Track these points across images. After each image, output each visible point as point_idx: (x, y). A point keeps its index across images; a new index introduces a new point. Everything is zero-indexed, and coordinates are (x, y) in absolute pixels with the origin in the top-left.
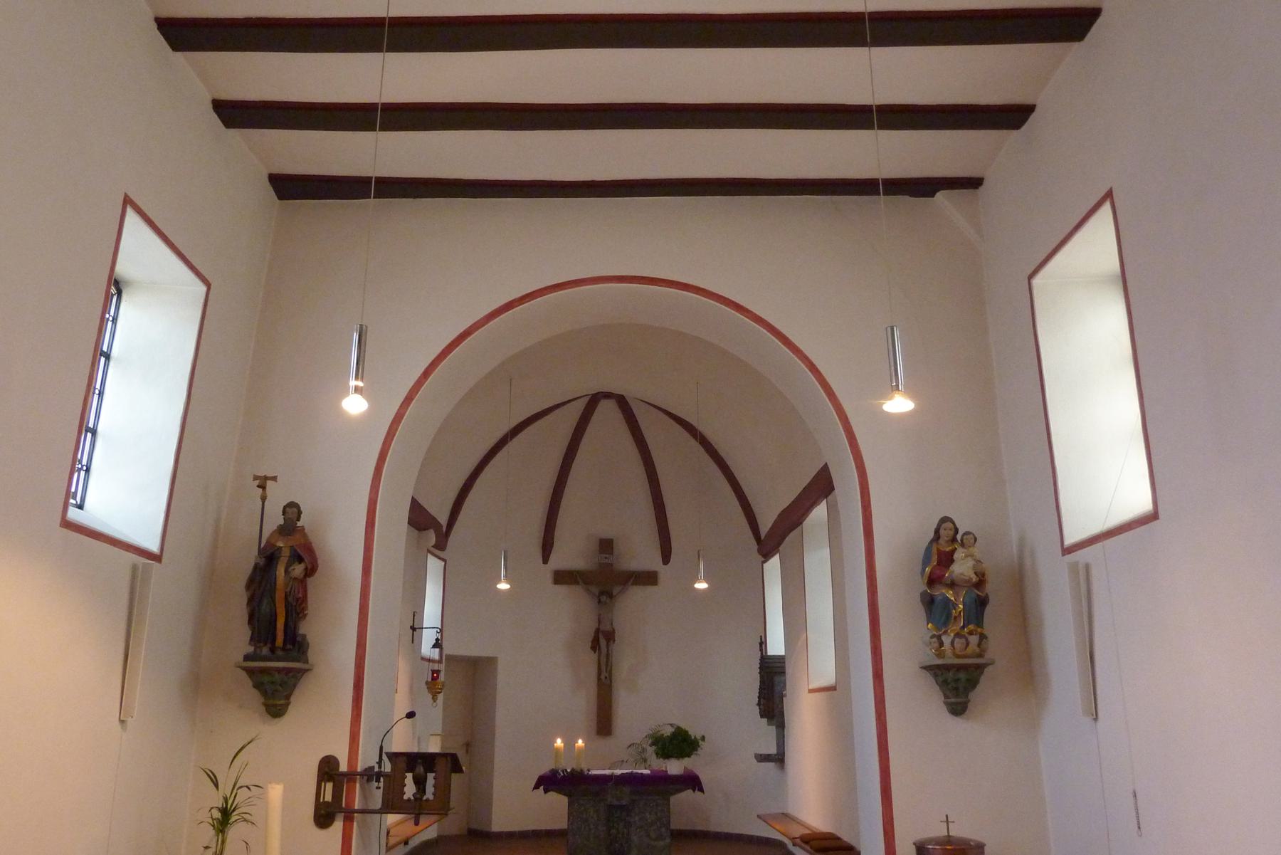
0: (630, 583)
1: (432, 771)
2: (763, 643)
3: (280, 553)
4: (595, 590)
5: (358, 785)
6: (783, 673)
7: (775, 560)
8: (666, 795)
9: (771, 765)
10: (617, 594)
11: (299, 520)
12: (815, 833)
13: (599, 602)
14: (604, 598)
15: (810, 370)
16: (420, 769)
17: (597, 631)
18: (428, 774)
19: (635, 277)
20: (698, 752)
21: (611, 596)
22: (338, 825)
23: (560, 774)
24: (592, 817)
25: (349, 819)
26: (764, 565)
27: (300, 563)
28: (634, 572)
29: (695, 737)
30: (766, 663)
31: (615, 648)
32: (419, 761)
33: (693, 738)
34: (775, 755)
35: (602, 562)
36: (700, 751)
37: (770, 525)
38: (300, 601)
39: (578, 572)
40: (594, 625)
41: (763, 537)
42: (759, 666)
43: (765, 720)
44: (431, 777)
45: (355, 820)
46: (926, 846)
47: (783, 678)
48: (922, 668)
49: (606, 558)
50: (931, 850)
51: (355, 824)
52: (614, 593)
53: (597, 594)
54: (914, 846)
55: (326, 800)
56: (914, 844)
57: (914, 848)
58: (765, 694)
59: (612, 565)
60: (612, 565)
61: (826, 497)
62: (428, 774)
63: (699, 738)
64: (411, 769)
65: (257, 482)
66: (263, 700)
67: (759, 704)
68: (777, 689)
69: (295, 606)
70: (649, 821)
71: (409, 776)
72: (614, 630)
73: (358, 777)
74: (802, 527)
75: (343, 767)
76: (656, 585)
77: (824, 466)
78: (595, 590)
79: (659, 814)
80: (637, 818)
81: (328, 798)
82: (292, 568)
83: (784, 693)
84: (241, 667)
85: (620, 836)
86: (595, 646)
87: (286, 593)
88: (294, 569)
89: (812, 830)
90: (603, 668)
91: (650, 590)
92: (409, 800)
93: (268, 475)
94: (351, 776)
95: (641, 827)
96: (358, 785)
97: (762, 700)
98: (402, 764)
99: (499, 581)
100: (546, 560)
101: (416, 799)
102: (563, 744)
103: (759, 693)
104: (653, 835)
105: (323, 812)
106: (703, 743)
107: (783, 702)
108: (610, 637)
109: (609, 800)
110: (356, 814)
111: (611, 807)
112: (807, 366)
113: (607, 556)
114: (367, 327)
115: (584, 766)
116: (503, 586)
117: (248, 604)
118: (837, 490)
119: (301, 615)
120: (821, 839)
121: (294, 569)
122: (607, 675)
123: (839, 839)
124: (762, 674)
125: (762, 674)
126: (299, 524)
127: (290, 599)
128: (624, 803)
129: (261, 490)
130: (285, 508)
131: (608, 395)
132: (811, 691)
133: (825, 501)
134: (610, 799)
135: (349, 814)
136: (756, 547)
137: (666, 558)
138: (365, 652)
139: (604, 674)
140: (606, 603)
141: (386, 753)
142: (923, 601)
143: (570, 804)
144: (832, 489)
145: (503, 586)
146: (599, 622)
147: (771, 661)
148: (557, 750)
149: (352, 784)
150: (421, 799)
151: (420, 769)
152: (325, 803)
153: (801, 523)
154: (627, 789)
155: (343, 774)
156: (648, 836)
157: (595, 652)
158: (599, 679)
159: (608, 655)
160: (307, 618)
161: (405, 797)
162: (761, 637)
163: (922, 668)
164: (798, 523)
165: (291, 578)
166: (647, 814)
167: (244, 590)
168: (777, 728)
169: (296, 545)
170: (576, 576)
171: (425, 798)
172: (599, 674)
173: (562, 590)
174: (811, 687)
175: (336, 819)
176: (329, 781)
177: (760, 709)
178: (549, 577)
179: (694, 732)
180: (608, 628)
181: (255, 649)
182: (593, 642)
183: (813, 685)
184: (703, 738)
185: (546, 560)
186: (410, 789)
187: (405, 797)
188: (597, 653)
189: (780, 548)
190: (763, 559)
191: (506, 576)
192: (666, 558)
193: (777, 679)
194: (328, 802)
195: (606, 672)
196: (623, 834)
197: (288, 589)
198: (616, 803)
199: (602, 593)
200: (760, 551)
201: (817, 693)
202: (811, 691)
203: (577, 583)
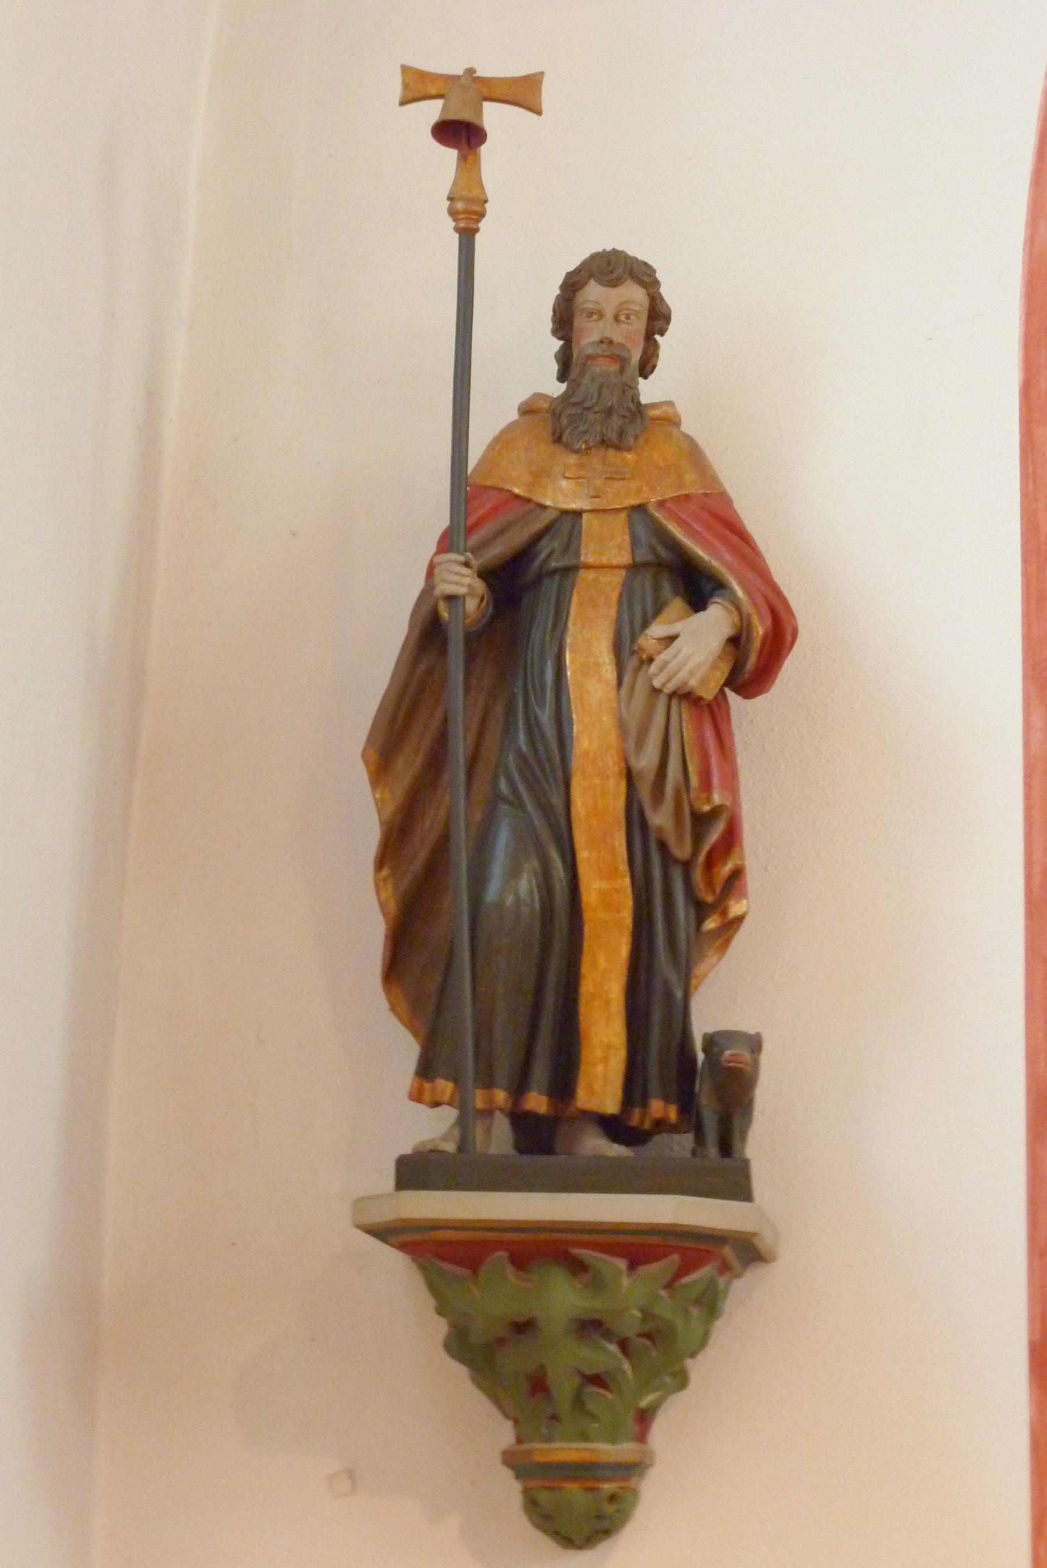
3: (572, 543)
11: (646, 368)
27: (697, 603)
38: (714, 835)
65: (432, 111)
66: (505, 1434)
69: (687, 866)
76: (752, 1202)
82: (658, 629)
84: (382, 1233)
87: (630, 776)
88: (672, 639)
93: (486, 70)
117: (380, 863)
119: (711, 924)
121: (672, 639)
126: (649, 391)
127: (660, 819)
129: (451, 154)
130: (572, 285)
142: (520, 1444)
160: (741, 938)
165: (656, 692)
167: (360, 775)
169: (661, 504)
181: (462, 1123)
197: (646, 761)
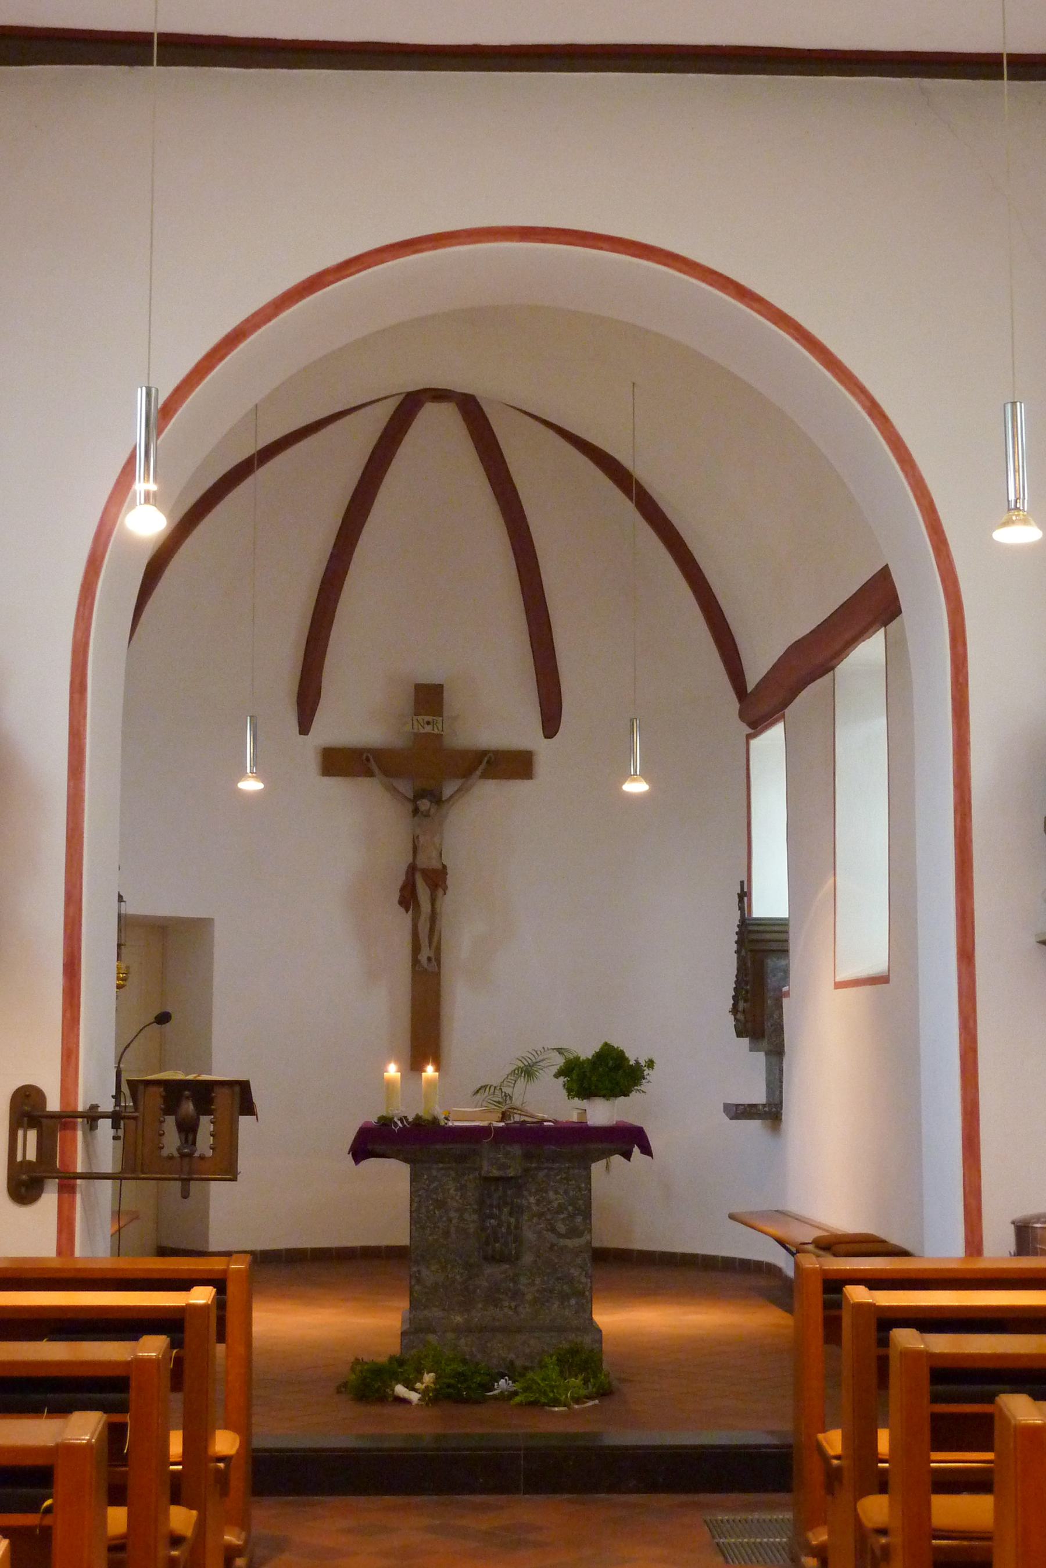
0: (478, 773)
1: (209, 1112)
2: (744, 896)
4: (405, 787)
5: (80, 1134)
6: (784, 952)
7: (774, 736)
8: (585, 1161)
9: (754, 1126)
10: (451, 797)
12: (836, 1236)
13: (416, 811)
14: (424, 804)
15: (870, 415)
16: (188, 1107)
17: (412, 869)
18: (201, 1117)
19: (548, 229)
20: (642, 1088)
21: (438, 800)
22: (49, 1199)
23: (396, 1124)
24: (452, 1198)
25: (67, 1184)
26: (754, 743)
28: (485, 753)
29: (637, 1062)
30: (750, 932)
31: (448, 903)
32: (187, 1093)
33: (632, 1062)
34: (764, 1105)
35: (422, 731)
36: (645, 1086)
37: (764, 671)
39: (369, 750)
40: (410, 860)
41: (750, 687)
42: (736, 938)
43: (745, 1041)
44: (205, 1121)
45: (78, 1189)
46: (1030, 1225)
47: (783, 962)
48: (1038, 942)
49: (428, 723)
50: (1039, 1232)
51: (78, 1197)
52: (447, 792)
53: (410, 795)
54: (1013, 1226)
55: (28, 1158)
56: (1013, 1223)
57: (1011, 1231)
58: (747, 992)
59: (439, 737)
60: (439, 737)
61: (885, 624)
62: (201, 1117)
63: (643, 1064)
64: (171, 1106)
67: (735, 1010)
68: (772, 982)
70: (555, 1204)
71: (170, 1122)
72: (444, 867)
73: (80, 1120)
74: (834, 674)
75: (53, 1104)
76: (531, 778)
77: (886, 566)
78: (405, 787)
79: (571, 1193)
80: (532, 1200)
81: (32, 1155)
83: (785, 989)
85: (504, 1230)
86: (408, 898)
89: (827, 1231)
90: (424, 941)
91: (519, 787)
92: (171, 1158)
94: (66, 1119)
95: (541, 1215)
96: (80, 1134)
97: (741, 1005)
98: (154, 1099)
99: (242, 775)
100: (304, 727)
101: (183, 1156)
102: (399, 1074)
103: (735, 989)
104: (561, 1228)
105: (24, 1177)
106: (650, 1072)
107: (781, 1007)
108: (437, 879)
109: (485, 1168)
110: (79, 1181)
111: (487, 1179)
112: (864, 407)
113: (430, 718)
114: (157, 390)
115: (439, 1112)
116: (251, 785)
118: (904, 614)
120: (849, 1243)
122: (432, 954)
123: (883, 1241)
124: (743, 953)
125: (743, 953)
128: (511, 1173)
131: (440, 395)
132: (839, 985)
133: (881, 633)
134: (485, 1166)
135: (66, 1181)
136: (736, 705)
137: (551, 723)
138: (80, 909)
139: (425, 953)
140: (427, 815)
141: (129, 1082)
143: (414, 1178)
144: (899, 612)
145: (251, 785)
146: (415, 850)
147: (761, 928)
148: (389, 1085)
149: (69, 1133)
150: (190, 1155)
151: (188, 1107)
152: (25, 1163)
153: (833, 668)
154: (516, 1150)
155: (53, 1116)
156: (553, 1230)
157: (407, 911)
158: (415, 961)
159: (434, 918)
161: (165, 1153)
162: (742, 883)
163: (1038, 942)
164: (826, 667)
166: (551, 1194)
168: (766, 1054)
170: (368, 760)
171: (196, 1155)
172: (416, 949)
173: (337, 787)
174: (838, 979)
175: (44, 1191)
176: (31, 1126)
177: (735, 1019)
178: (312, 763)
179: (633, 1055)
180: (435, 864)
182: (402, 889)
183: (843, 976)
184: (651, 1064)
185: (304, 727)
186: (172, 1141)
187: (165, 1153)
188: (410, 912)
189: (786, 711)
190: (750, 731)
191: (255, 762)
192: (551, 723)
193: (771, 963)
194: (30, 1162)
195: (430, 946)
196: (509, 1227)
198: (495, 1173)
199: (419, 795)
200: (742, 715)
201: (854, 989)
202: (839, 985)
203: (369, 773)
